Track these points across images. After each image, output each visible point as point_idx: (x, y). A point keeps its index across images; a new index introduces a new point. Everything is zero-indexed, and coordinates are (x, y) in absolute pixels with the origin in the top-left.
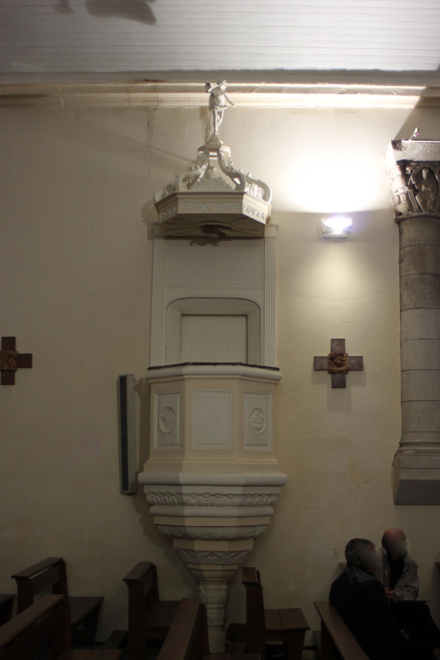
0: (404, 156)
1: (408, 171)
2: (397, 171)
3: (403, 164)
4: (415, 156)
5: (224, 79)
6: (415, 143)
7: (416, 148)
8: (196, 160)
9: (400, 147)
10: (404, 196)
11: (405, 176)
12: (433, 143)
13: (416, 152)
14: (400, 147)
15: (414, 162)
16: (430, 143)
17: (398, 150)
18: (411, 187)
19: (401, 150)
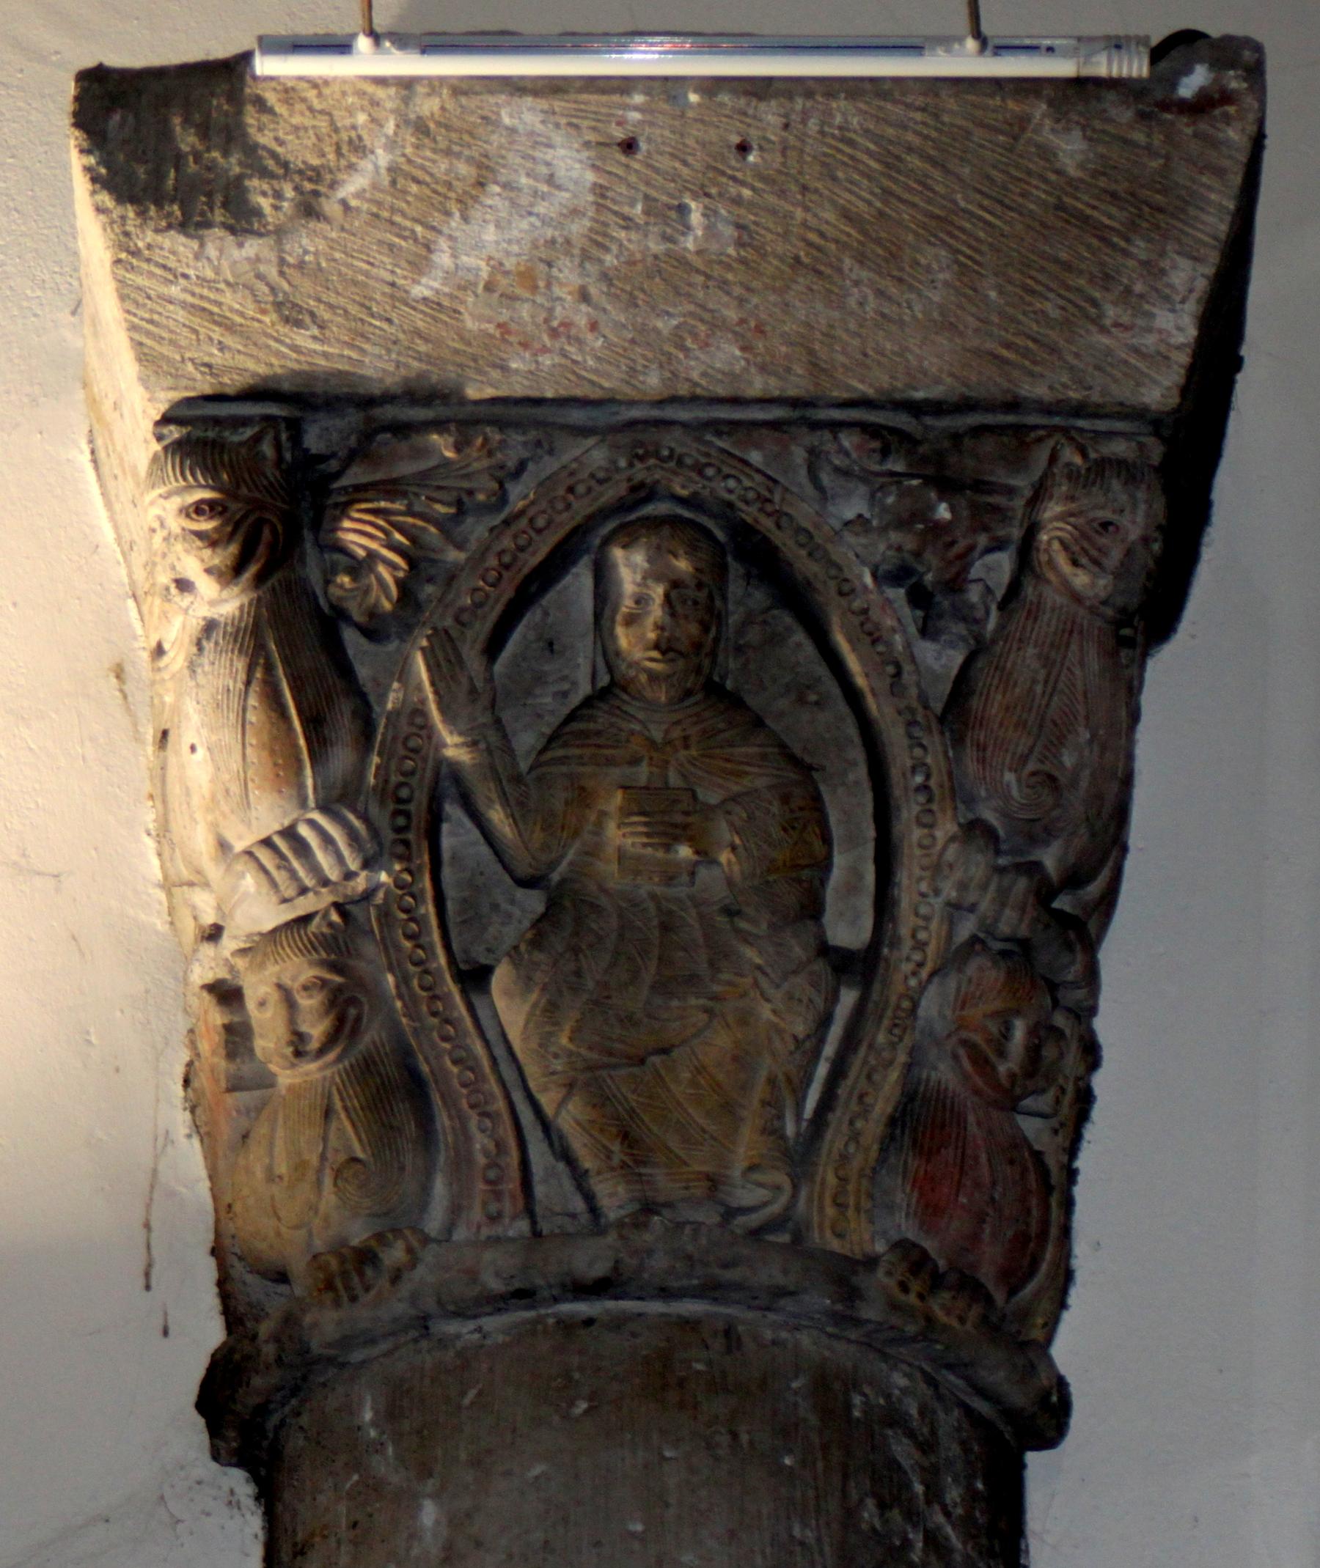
0: (292, 314)
1: (360, 567)
2: (141, 565)
3: (268, 469)
4: (475, 318)
5: (1177, 410)
6: (462, 87)
7: (485, 174)
8: (801, 1036)
9: (233, 165)
10: (298, 969)
11: (304, 657)
12: (759, 88)
13: (483, 242)
14: (233, 165)
15: (470, 420)
16: (712, 86)
17: (190, 224)
18: (407, 814)
19: (242, 220)
